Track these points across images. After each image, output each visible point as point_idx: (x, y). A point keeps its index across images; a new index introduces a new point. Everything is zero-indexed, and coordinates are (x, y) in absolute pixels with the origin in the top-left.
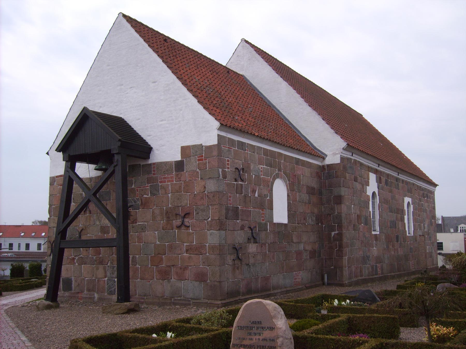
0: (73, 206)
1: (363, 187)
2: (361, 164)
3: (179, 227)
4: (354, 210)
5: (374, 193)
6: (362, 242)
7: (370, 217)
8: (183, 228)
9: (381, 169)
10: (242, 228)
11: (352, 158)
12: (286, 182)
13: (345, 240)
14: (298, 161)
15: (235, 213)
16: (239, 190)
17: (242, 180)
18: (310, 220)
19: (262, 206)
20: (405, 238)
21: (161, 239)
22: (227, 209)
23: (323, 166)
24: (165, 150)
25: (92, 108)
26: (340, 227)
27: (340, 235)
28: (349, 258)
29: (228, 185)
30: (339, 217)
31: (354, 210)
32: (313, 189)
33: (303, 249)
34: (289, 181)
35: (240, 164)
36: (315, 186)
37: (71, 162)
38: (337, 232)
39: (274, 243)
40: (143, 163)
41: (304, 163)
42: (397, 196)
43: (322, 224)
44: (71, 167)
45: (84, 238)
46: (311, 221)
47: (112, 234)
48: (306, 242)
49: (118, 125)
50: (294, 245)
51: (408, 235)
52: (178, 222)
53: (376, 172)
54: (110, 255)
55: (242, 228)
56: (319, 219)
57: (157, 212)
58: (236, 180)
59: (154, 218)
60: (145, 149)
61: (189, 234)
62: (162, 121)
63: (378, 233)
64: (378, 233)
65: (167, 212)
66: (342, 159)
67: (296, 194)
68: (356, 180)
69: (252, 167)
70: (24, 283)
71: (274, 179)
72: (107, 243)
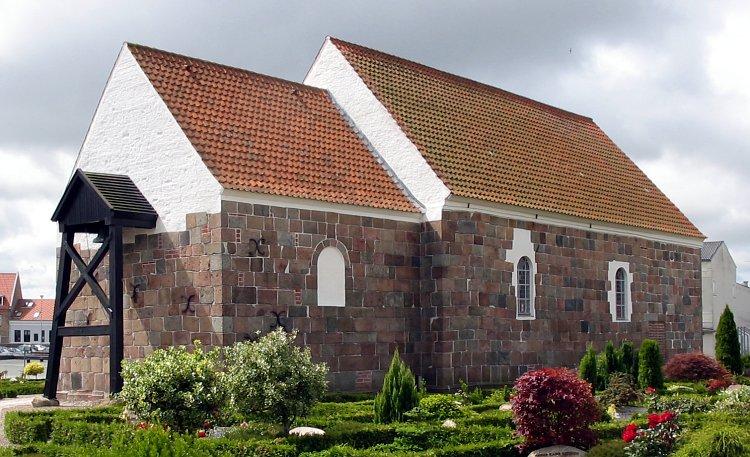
0: (72, 286)
1: (496, 250)
2: (493, 219)
3: (184, 312)
4: (471, 287)
5: (524, 261)
6: (490, 332)
7: (513, 294)
8: (188, 313)
9: (541, 220)
10: (261, 313)
11: (468, 210)
12: (343, 251)
13: (448, 329)
14: (368, 221)
15: (250, 296)
16: (257, 266)
17: (263, 255)
18: (392, 301)
19: (296, 284)
20: (606, 325)
21: (167, 325)
22: (236, 291)
23: (422, 224)
24: (171, 221)
25: (89, 168)
26: (440, 311)
27: (440, 321)
28: (456, 356)
29: (236, 261)
30: (439, 296)
31: (471, 287)
32: (401, 257)
33: (375, 340)
34: (349, 249)
35: (258, 234)
36: (404, 254)
37: (68, 233)
38: (436, 318)
39: (318, 332)
40: (149, 232)
41: (379, 223)
42: (587, 261)
43: (418, 305)
44: (68, 238)
45: (93, 324)
46: (395, 302)
47: (102, 318)
48: (386, 328)
49: (122, 187)
50: (358, 336)
51: (614, 320)
52: (182, 306)
53: (531, 226)
54: (102, 343)
55: (261, 313)
56: (413, 299)
57: (163, 293)
58: (251, 254)
59: (160, 302)
60: (152, 219)
61: (194, 320)
62: (168, 181)
63: (534, 318)
64: (534, 318)
65: (173, 294)
66: (445, 214)
67: (363, 267)
68: (478, 241)
69: (279, 237)
70: (479, 422)
71: (320, 248)
72: (98, 331)
